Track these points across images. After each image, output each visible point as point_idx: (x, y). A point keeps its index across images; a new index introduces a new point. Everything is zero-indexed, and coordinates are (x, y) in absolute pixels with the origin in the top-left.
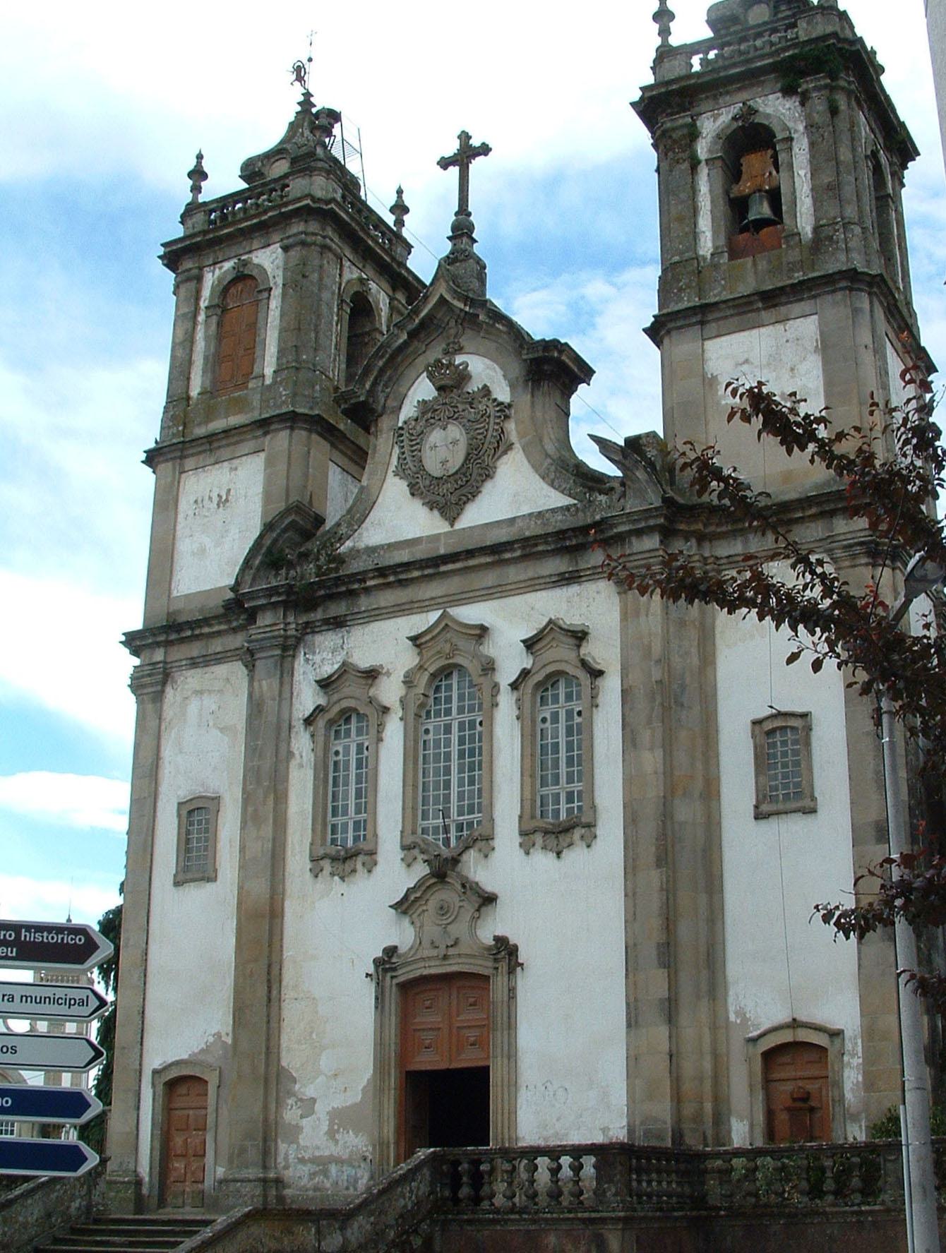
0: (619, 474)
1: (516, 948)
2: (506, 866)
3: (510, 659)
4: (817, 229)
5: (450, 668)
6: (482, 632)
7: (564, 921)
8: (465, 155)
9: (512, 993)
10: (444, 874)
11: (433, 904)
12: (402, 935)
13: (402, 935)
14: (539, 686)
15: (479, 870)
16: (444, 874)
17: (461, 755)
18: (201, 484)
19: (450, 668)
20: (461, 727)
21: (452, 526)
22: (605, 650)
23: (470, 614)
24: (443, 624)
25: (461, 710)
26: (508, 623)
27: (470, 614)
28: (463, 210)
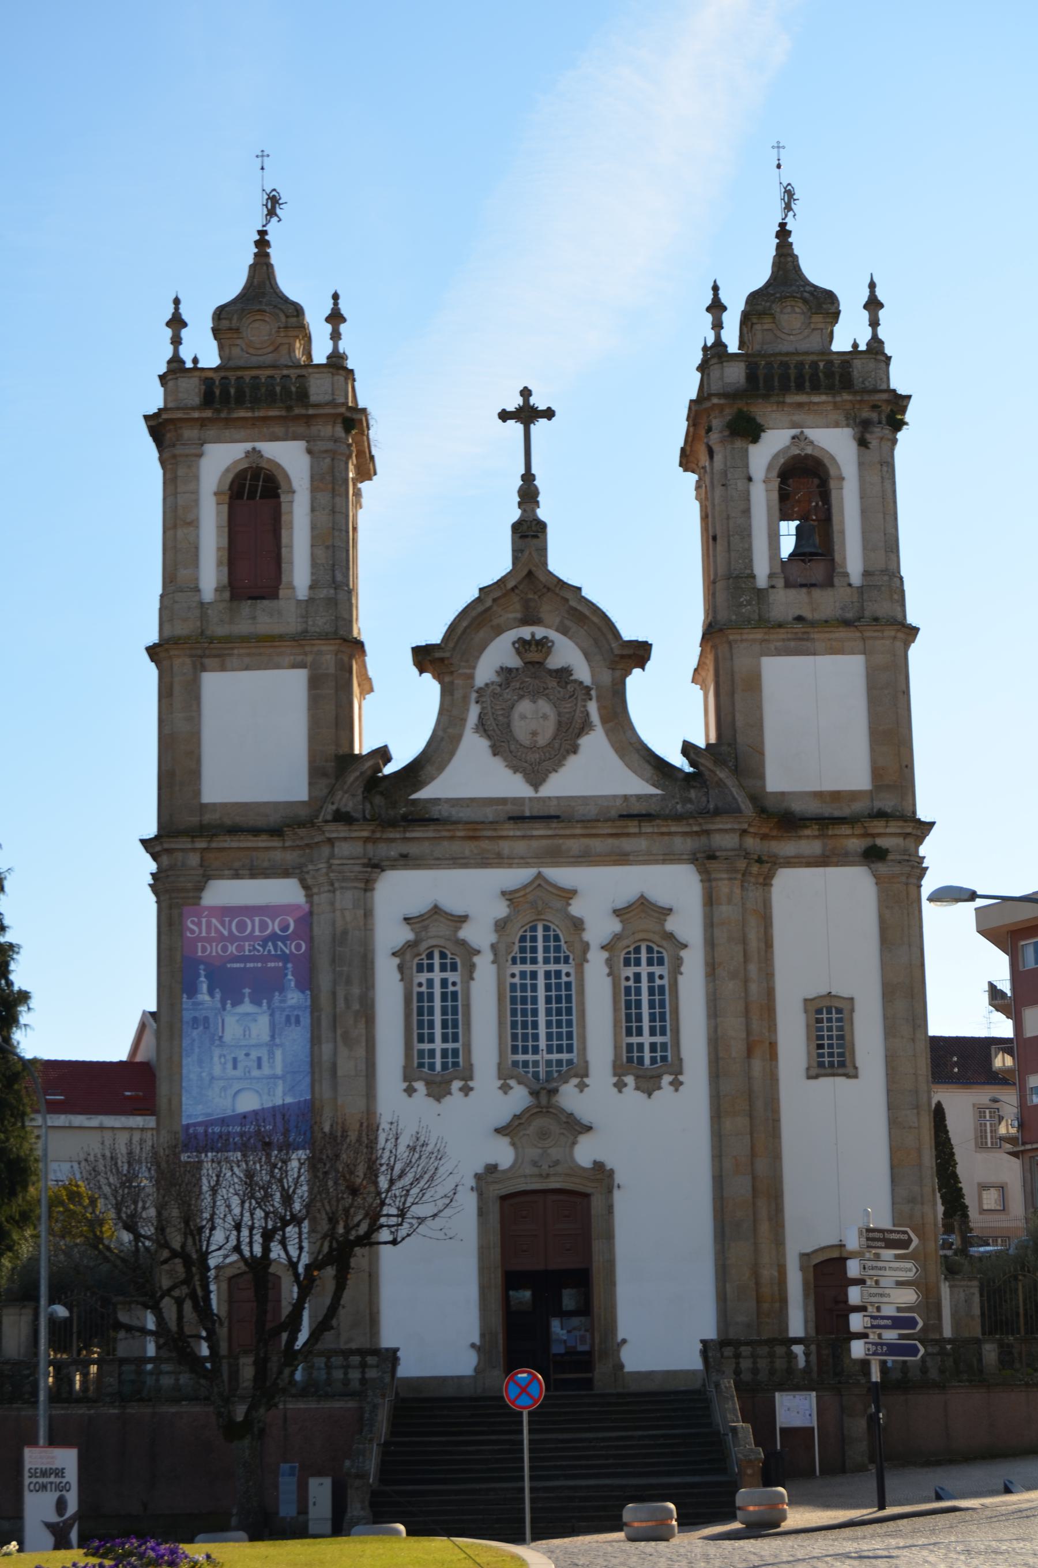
0: (688, 769)
1: (611, 1173)
2: (598, 1098)
3: (600, 927)
4: (866, 574)
5: (539, 926)
6: (568, 894)
7: (653, 1152)
8: (527, 414)
9: (610, 1209)
10: (545, 1118)
11: (531, 1130)
12: (503, 1154)
13: (503, 1154)
14: (623, 952)
15: (569, 1097)
16: (545, 1118)
17: (548, 1000)
18: (222, 690)
19: (539, 926)
20: (548, 975)
21: (536, 791)
22: (688, 924)
23: (562, 875)
24: (535, 885)
25: (546, 961)
26: (599, 892)
27: (562, 875)
28: (528, 477)
